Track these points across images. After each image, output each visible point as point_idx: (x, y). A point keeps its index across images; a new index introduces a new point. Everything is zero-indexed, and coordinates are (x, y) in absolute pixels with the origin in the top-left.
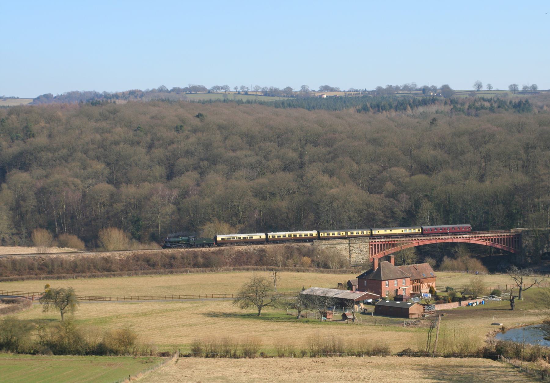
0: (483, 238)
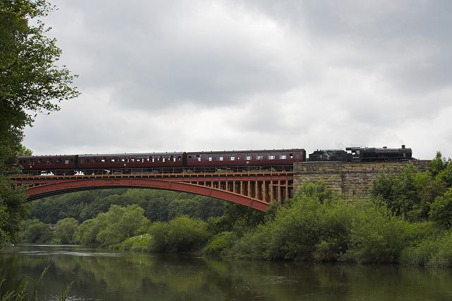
0: (201, 180)
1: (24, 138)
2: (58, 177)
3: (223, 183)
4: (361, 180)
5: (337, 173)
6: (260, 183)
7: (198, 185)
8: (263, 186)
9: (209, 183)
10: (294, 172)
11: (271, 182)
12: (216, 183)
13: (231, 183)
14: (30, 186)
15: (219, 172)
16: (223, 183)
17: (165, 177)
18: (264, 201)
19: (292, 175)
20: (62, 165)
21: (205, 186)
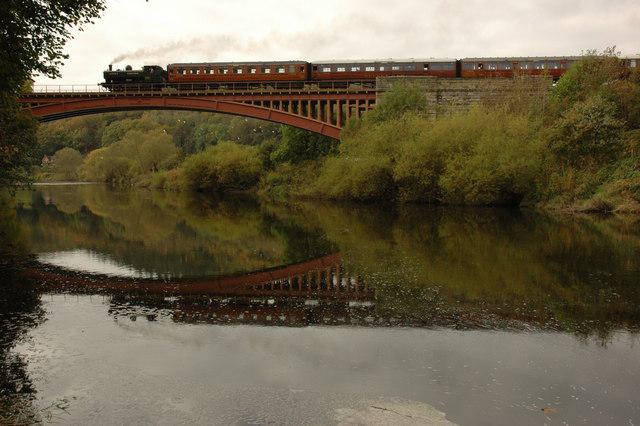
1: (41, 328)
2: (116, 94)
3: (286, 103)
4: (461, 101)
5: (432, 91)
6: (314, 103)
7: (243, 103)
8: (318, 106)
9: (258, 103)
10: (377, 89)
11: (348, 102)
12: (276, 103)
13: (295, 103)
14: (246, 102)
15: (354, 87)
16: (286, 103)
17: (237, 94)
18: (299, 115)
19: (374, 93)
20: (41, 96)
21: (262, 106)
